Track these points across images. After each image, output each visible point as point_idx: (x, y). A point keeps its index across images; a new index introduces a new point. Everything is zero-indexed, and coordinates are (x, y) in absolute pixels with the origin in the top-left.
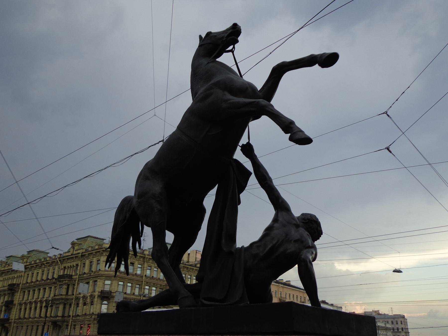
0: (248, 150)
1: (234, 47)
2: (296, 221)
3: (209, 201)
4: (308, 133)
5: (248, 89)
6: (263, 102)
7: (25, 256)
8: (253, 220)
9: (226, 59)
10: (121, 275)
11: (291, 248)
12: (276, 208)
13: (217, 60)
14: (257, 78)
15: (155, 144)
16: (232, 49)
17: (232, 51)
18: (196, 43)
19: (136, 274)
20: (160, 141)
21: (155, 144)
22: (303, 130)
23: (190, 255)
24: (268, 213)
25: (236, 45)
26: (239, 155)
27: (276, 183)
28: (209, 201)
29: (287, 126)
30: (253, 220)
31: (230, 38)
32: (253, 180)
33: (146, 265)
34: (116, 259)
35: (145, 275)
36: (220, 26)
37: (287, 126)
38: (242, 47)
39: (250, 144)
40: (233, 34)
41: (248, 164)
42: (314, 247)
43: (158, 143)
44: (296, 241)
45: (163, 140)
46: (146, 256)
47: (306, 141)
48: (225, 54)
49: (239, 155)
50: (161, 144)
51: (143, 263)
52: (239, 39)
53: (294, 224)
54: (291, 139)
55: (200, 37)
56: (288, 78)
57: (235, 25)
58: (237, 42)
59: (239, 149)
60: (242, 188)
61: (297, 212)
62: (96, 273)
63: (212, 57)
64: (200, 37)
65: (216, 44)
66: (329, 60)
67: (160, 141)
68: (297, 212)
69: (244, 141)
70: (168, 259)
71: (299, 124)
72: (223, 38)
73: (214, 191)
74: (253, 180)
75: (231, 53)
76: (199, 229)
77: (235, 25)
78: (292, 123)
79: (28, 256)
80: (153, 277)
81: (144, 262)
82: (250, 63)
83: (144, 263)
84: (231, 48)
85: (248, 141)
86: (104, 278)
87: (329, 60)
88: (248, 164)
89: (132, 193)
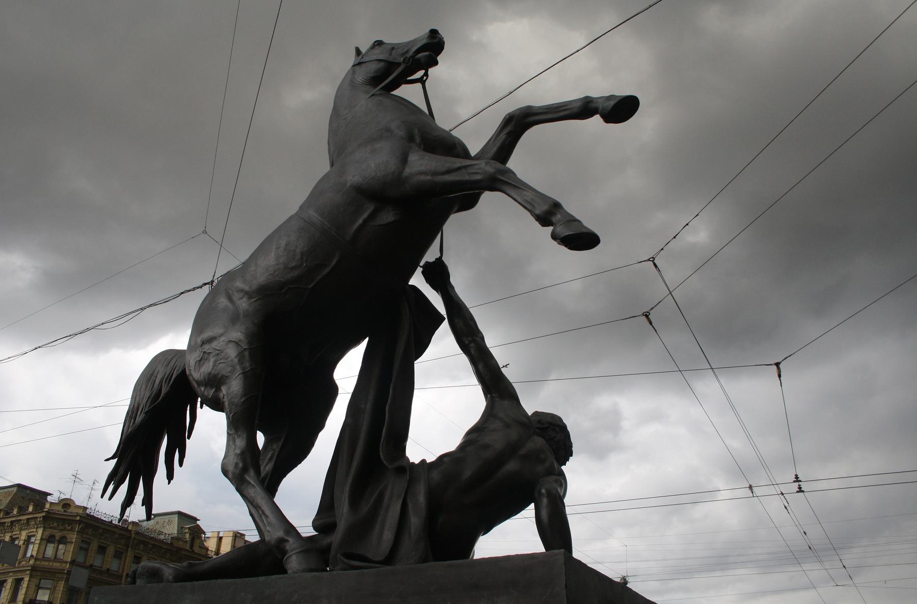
0: (438, 275)
1: (426, 74)
3: (348, 371)
4: (591, 224)
5: (450, 147)
8: (442, 411)
9: (409, 92)
12: (487, 391)
13: (395, 92)
15: (194, 289)
16: (422, 77)
17: (422, 81)
19: (108, 570)
20: (206, 284)
21: (194, 289)
22: (578, 218)
25: (430, 71)
26: (417, 280)
28: (348, 371)
29: (548, 214)
30: (442, 411)
32: (444, 341)
36: (406, 33)
37: (548, 214)
38: (441, 73)
39: (443, 262)
40: (432, 48)
43: (201, 287)
45: (212, 282)
48: (404, 87)
49: (417, 280)
50: (206, 290)
54: (554, 237)
55: (358, 52)
58: (436, 63)
59: (419, 270)
60: (420, 347)
62: (58, 535)
64: (358, 52)
67: (206, 284)
69: (430, 256)
70: (257, 474)
71: (572, 207)
73: (367, 339)
74: (444, 341)
75: (419, 85)
76: (320, 425)
77: (434, 33)
83: (127, 550)
85: (438, 255)
86: (39, 574)
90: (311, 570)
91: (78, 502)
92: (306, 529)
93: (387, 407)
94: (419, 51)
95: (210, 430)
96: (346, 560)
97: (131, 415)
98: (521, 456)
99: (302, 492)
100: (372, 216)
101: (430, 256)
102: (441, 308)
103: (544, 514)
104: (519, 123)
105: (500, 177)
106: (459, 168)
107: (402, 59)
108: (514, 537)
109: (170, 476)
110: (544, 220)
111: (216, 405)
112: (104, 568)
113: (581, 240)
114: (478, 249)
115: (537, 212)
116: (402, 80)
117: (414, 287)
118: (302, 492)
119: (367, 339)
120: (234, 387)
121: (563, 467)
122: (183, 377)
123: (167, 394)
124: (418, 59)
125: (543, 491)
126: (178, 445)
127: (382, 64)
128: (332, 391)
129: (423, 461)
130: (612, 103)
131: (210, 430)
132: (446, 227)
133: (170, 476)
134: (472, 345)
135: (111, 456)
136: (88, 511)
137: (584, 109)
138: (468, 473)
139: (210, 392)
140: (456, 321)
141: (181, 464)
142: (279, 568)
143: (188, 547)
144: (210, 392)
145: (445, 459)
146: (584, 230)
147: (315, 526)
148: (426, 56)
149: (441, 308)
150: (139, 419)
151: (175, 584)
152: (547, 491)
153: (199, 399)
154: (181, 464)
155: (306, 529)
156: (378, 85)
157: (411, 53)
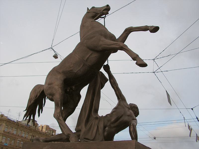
0: (107, 68)
1: (105, 16)
2: (128, 106)
3: (84, 92)
5: (112, 37)
6: (121, 44)
8: (107, 103)
9: (100, 21)
11: (126, 118)
12: (118, 98)
16: (104, 17)
18: (86, 11)
24: (115, 102)
26: (102, 70)
27: (120, 86)
28: (84, 92)
29: (135, 57)
30: (107, 103)
31: (105, 11)
32: (108, 85)
33: (19, 130)
34: (29, 117)
36: (100, 5)
37: (135, 57)
40: (107, 9)
41: (107, 75)
42: (136, 120)
44: (128, 116)
47: (144, 65)
48: (100, 19)
49: (102, 70)
53: (128, 108)
54: (136, 64)
55: (88, 9)
56: (132, 35)
57: (108, 5)
59: (103, 67)
60: (102, 86)
63: (94, 19)
64: (88, 9)
65: (96, 14)
68: (129, 102)
69: (106, 64)
72: (101, 10)
74: (108, 85)
77: (108, 5)
78: (137, 56)
82: (114, 25)
84: (104, 16)
87: (155, 29)
88: (107, 75)
89: (43, 82)
90: (76, 141)
91: (5, 115)
92: (74, 131)
93: (94, 102)
94: (104, 10)
95: (49, 106)
96: (84, 140)
97: (30, 100)
98: (126, 115)
99: (72, 122)
100: (91, 55)
101: (106, 64)
102: (108, 78)
103: (132, 129)
104: (128, 31)
105: (124, 47)
106: (114, 44)
107: (99, 13)
108: (123, 135)
109: (39, 116)
110: (134, 59)
111: (52, 100)
112: (8, 131)
113: (143, 65)
114: (117, 62)
115: (133, 57)
116: (100, 17)
117: (101, 72)
118: (72, 122)
119: (88, 85)
120: (58, 96)
121: (136, 118)
122: (43, 92)
123: (39, 96)
124: (104, 13)
125: (131, 124)
126: (41, 108)
127: (95, 13)
128: (80, 97)
129: (102, 116)
130: (153, 28)
131: (49, 106)
132: (109, 58)
133: (39, 116)
134: (115, 87)
135: (25, 110)
136: (8, 118)
137: (145, 29)
138: (113, 120)
139: (51, 97)
140: (111, 80)
141: (42, 113)
142: (68, 140)
143: (34, 129)
144: (51, 97)
145: (108, 116)
146: (144, 63)
147: (76, 130)
148: (106, 12)
149: (108, 78)
150: (32, 102)
151: (43, 143)
152: (132, 124)
153: (46, 97)
154: (42, 113)
155: (74, 131)
156: (94, 18)
157: (102, 11)
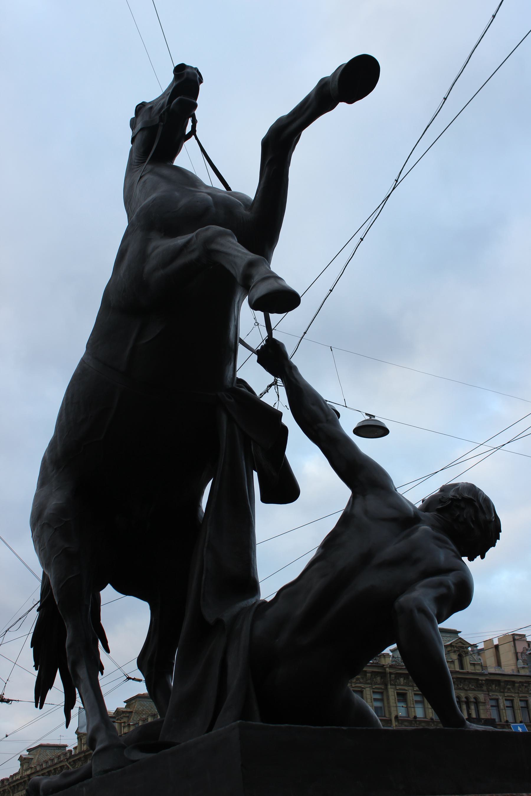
7: (123, 712)
9: (188, 158)
10: (403, 727)
14: (245, 180)
20: (270, 386)
23: (501, 648)
33: (392, 693)
35: (396, 717)
36: (156, 85)
41: (277, 399)
46: (388, 670)
51: (382, 687)
52: (198, 102)
61: (415, 489)
66: (357, 78)
67: (270, 386)
79: (129, 710)
80: (415, 717)
81: (386, 685)
83: (386, 689)
87: (357, 78)
